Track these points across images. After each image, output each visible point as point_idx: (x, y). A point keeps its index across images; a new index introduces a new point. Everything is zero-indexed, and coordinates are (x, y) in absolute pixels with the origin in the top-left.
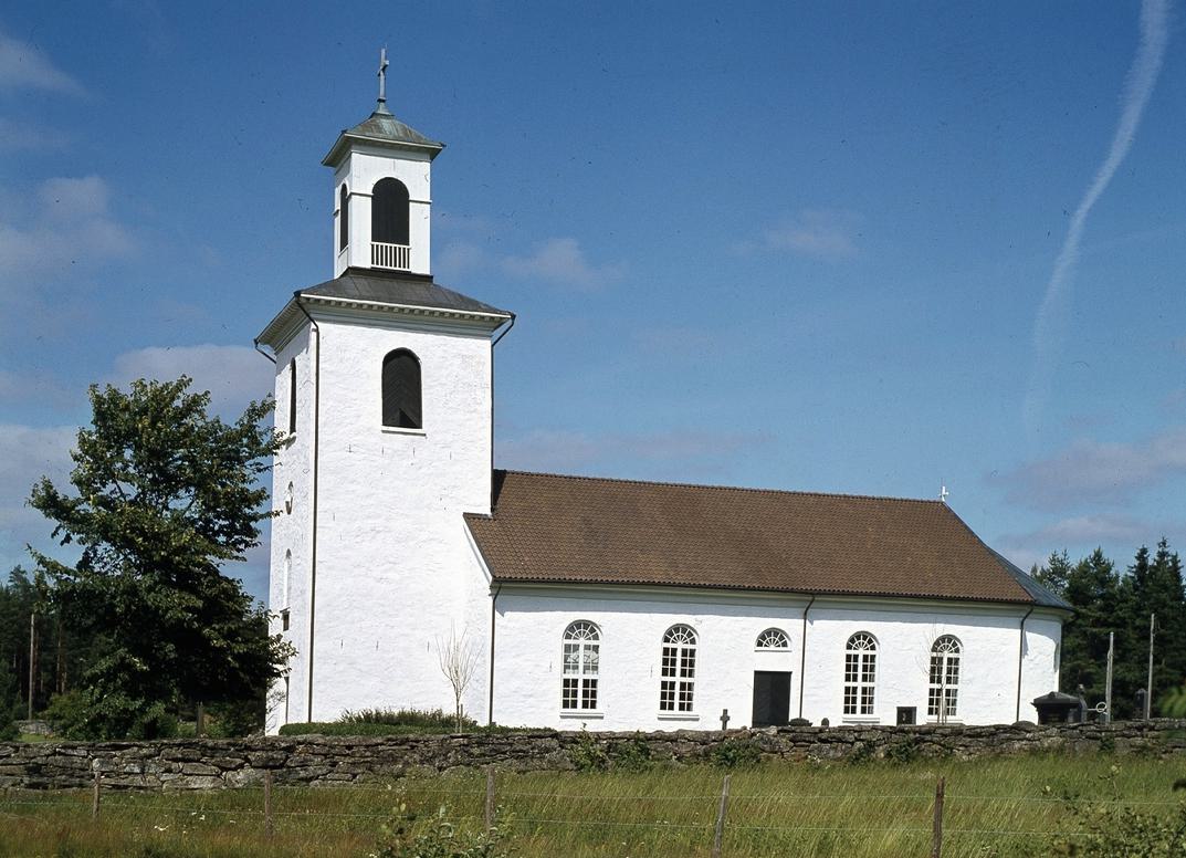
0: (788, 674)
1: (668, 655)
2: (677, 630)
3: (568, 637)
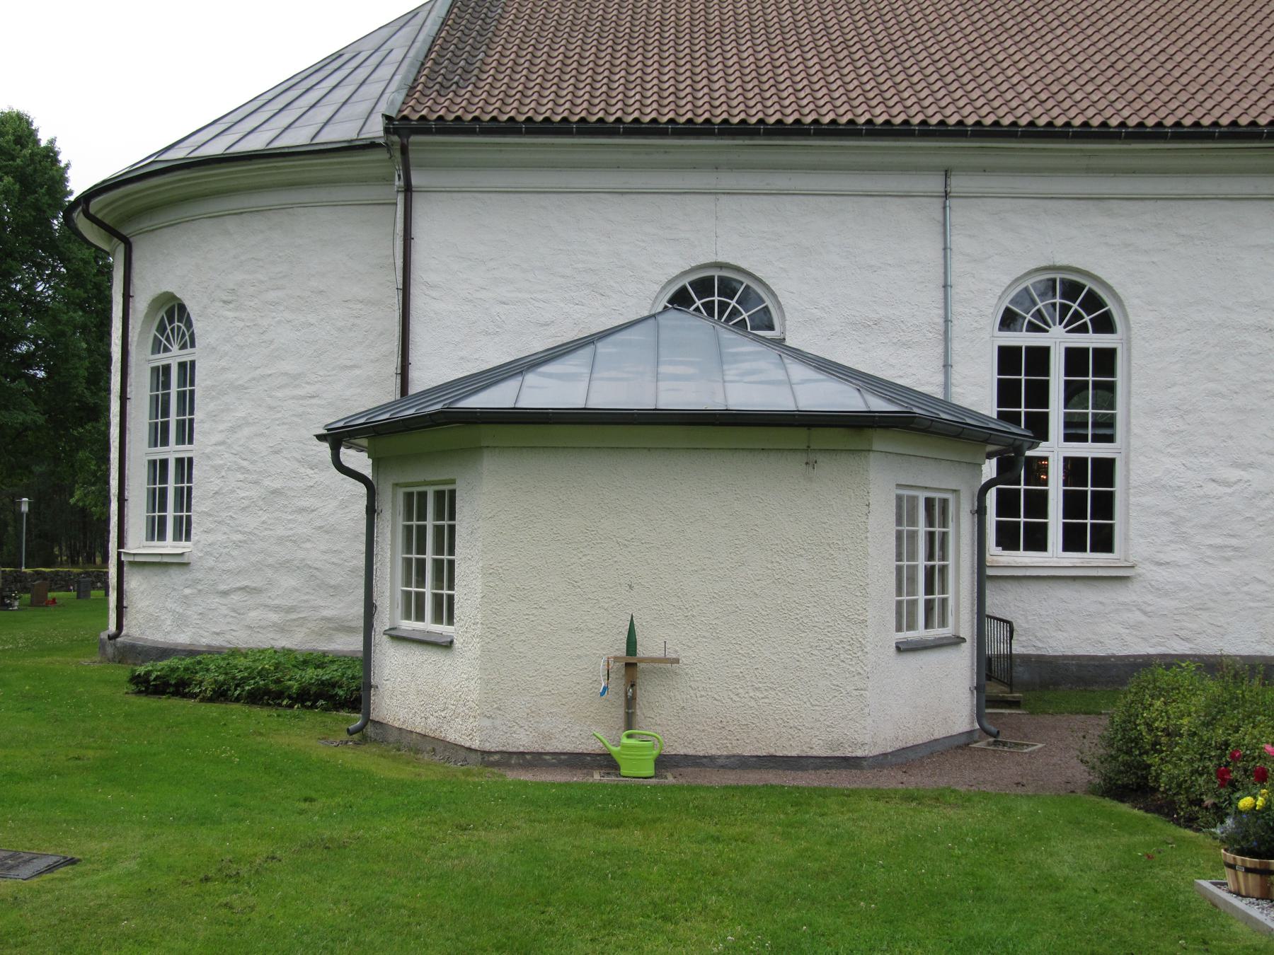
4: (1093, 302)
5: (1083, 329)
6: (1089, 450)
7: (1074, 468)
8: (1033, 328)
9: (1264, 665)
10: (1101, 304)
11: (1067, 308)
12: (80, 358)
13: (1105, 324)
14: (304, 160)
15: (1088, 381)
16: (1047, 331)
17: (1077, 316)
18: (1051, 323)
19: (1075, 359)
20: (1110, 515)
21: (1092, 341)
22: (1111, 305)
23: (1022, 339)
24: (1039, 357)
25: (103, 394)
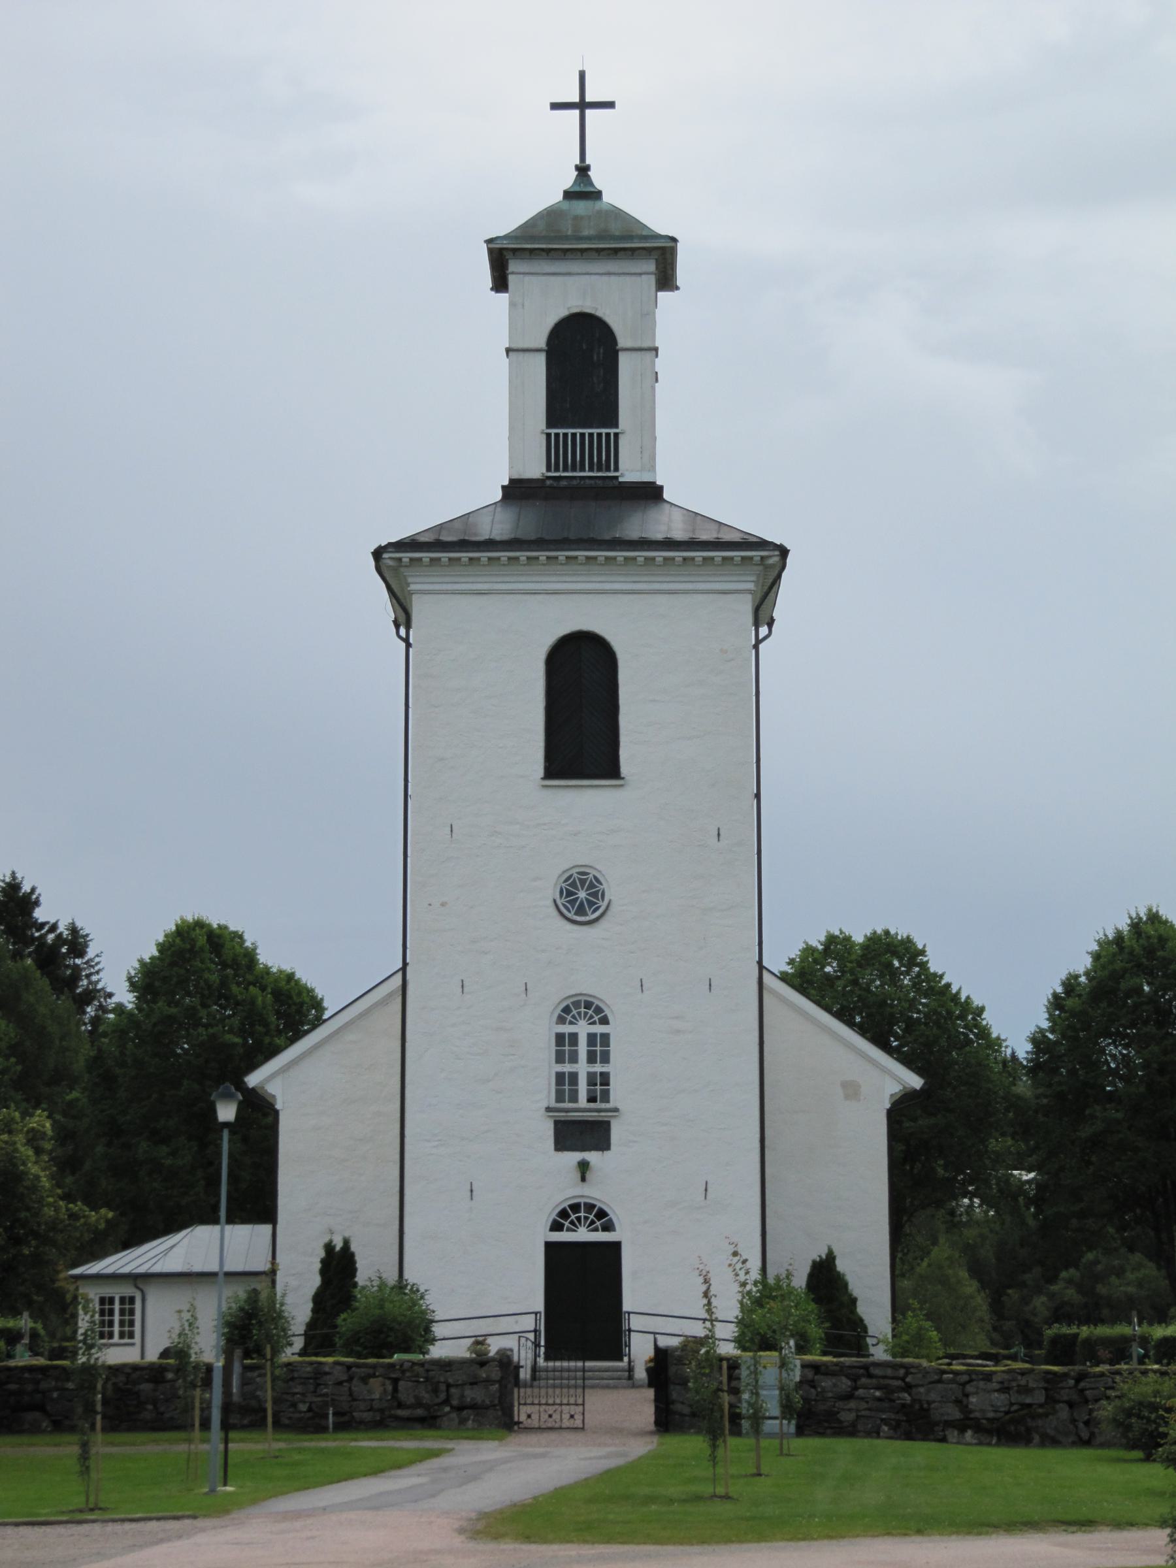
0: (608, 1101)
1: (564, 1045)
2: (577, 1004)
3: (561, 1020)
4: (599, 1010)
5: (594, 1023)
6: (598, 1068)
7: (574, 1059)
8: (571, 1023)
9: (264, 965)
10: (592, 1003)
11: (593, 1017)
12: (17, 1123)
13: (605, 1021)
14: (590, 1116)
15: (601, 1046)
16: (576, 1024)
17: (591, 1017)
18: (578, 1018)
19: (592, 1038)
20: (557, 1051)
21: (599, 1029)
22: (597, 1002)
23: (566, 1029)
24: (574, 1038)
25: (219, 1142)
